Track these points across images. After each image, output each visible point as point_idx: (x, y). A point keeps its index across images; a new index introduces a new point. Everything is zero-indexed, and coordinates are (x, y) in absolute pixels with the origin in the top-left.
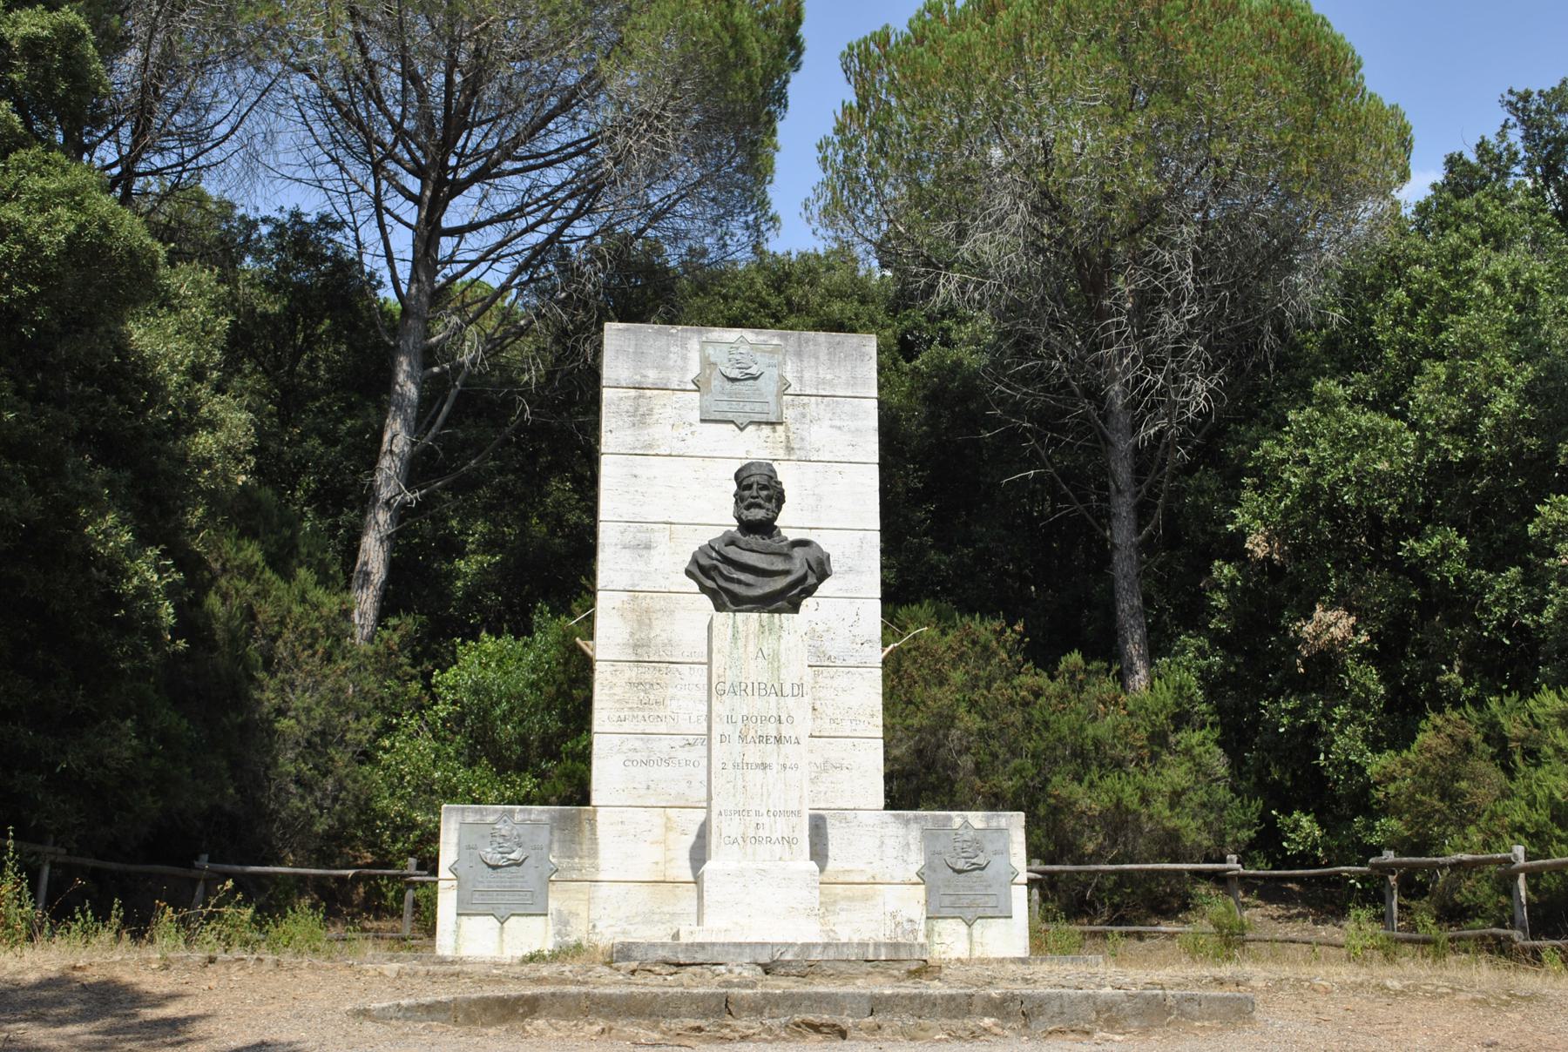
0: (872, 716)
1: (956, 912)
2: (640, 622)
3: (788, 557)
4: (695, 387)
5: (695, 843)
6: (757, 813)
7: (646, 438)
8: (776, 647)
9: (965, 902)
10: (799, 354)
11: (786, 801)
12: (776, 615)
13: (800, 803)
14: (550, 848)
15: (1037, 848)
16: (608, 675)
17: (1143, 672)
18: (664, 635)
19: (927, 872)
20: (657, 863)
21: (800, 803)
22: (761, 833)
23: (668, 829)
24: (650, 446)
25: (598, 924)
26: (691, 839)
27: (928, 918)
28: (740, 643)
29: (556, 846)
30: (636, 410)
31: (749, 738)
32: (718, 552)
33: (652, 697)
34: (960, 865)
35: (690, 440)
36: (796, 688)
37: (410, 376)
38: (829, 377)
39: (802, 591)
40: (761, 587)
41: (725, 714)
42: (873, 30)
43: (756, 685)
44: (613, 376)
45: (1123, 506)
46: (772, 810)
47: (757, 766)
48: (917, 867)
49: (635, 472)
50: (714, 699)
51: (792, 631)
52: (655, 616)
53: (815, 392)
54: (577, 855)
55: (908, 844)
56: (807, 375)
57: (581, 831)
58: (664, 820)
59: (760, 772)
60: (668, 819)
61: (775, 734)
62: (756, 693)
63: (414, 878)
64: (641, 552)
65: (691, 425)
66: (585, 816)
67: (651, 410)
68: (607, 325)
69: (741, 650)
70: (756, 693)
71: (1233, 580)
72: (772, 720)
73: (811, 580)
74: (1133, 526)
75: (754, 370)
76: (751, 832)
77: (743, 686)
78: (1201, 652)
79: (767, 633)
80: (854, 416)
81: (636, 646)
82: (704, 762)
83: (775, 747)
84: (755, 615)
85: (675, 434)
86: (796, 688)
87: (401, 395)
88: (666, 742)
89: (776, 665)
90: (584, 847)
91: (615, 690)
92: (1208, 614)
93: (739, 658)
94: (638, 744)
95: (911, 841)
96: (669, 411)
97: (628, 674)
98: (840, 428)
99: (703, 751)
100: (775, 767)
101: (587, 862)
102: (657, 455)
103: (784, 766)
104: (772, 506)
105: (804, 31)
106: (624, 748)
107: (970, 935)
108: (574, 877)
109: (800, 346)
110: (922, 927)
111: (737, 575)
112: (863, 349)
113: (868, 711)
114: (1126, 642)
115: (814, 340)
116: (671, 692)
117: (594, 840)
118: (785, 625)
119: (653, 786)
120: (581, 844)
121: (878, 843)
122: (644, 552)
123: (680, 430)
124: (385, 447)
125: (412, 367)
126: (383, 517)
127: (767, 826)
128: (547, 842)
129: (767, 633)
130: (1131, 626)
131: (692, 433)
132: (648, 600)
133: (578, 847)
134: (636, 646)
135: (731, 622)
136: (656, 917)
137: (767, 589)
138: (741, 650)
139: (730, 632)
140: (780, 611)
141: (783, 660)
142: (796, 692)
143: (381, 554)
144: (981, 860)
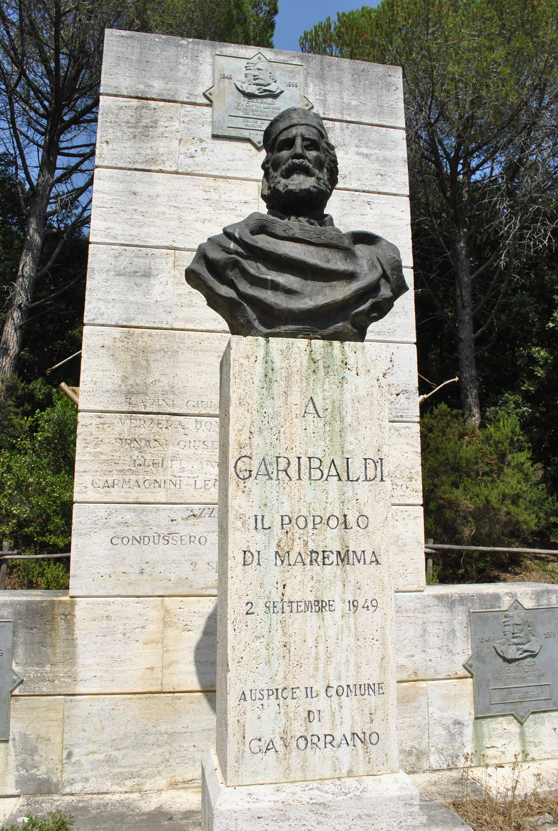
0: (411, 479)
1: (508, 709)
2: (135, 364)
3: (349, 254)
4: (206, 101)
5: (201, 641)
6: (309, 692)
7: (149, 151)
8: (336, 396)
9: (517, 696)
10: (322, 77)
11: (358, 666)
12: (336, 344)
13: (383, 669)
14: (12, 653)
15: (430, 531)
16: (93, 429)
17: (477, 415)
18: (165, 380)
19: (475, 663)
20: (152, 669)
21: (383, 669)
22: (316, 728)
23: (166, 624)
24: (153, 160)
25: (76, 751)
26: (195, 636)
27: (477, 718)
28: (277, 389)
29: (20, 650)
30: (138, 121)
31: (293, 556)
32: (239, 241)
33: (148, 457)
34: (512, 653)
35: (200, 158)
36: (371, 465)
37: (36, 230)
38: (354, 103)
39: (373, 308)
40: (310, 297)
41: (250, 514)
42: (315, 25)
43: (304, 460)
44: (113, 83)
45: (467, 316)
46: (334, 684)
47: (308, 606)
48: (462, 659)
49: (134, 188)
50: (232, 488)
51: (361, 371)
52: (153, 357)
53: (339, 117)
54: (49, 662)
55: (453, 631)
56: (330, 99)
57: (53, 629)
58: (162, 612)
59: (312, 617)
60: (167, 611)
61: (336, 546)
62: (305, 476)
63: (7, 557)
64: (139, 281)
65: (201, 141)
66: (59, 610)
67: (156, 122)
68: (107, 31)
69: (279, 402)
70: (305, 476)
71: (546, 359)
72: (333, 522)
73: (385, 292)
74: (471, 328)
75: (273, 87)
76: (298, 729)
77: (283, 463)
78: (517, 405)
79: (321, 372)
80: (382, 145)
81: (129, 394)
82: (214, 538)
83: (337, 570)
84: (302, 343)
85: (183, 149)
86: (371, 465)
87: (31, 242)
88: (165, 512)
89: (337, 426)
90: (58, 650)
91: (104, 448)
92: (521, 381)
93: (276, 414)
94: (129, 517)
95: (457, 627)
96: (176, 125)
97: (118, 427)
98: (367, 156)
99: (213, 524)
100: (339, 606)
101: (61, 670)
102: (161, 171)
103: (354, 604)
104: (324, 175)
105: (277, 19)
106: (112, 522)
107: (522, 735)
108: (45, 690)
109: (322, 69)
110: (469, 731)
111: (283, 279)
112: (389, 79)
113: (406, 473)
114: (467, 397)
115: (337, 65)
116: (172, 450)
117: (71, 641)
118: (351, 361)
119: (147, 570)
120: (53, 646)
121: (419, 631)
122: (143, 281)
123: (189, 145)
124: (20, 273)
125: (38, 226)
126: (16, 314)
127: (326, 716)
128: (9, 645)
129: (321, 372)
130: (471, 388)
131: (203, 150)
132: (146, 338)
133: (49, 651)
134: (129, 394)
135: (261, 353)
136: (151, 739)
137: (321, 300)
138: (279, 402)
139: (259, 369)
140: (341, 337)
141: (348, 419)
142: (371, 473)
143: (15, 338)
144: (534, 646)
